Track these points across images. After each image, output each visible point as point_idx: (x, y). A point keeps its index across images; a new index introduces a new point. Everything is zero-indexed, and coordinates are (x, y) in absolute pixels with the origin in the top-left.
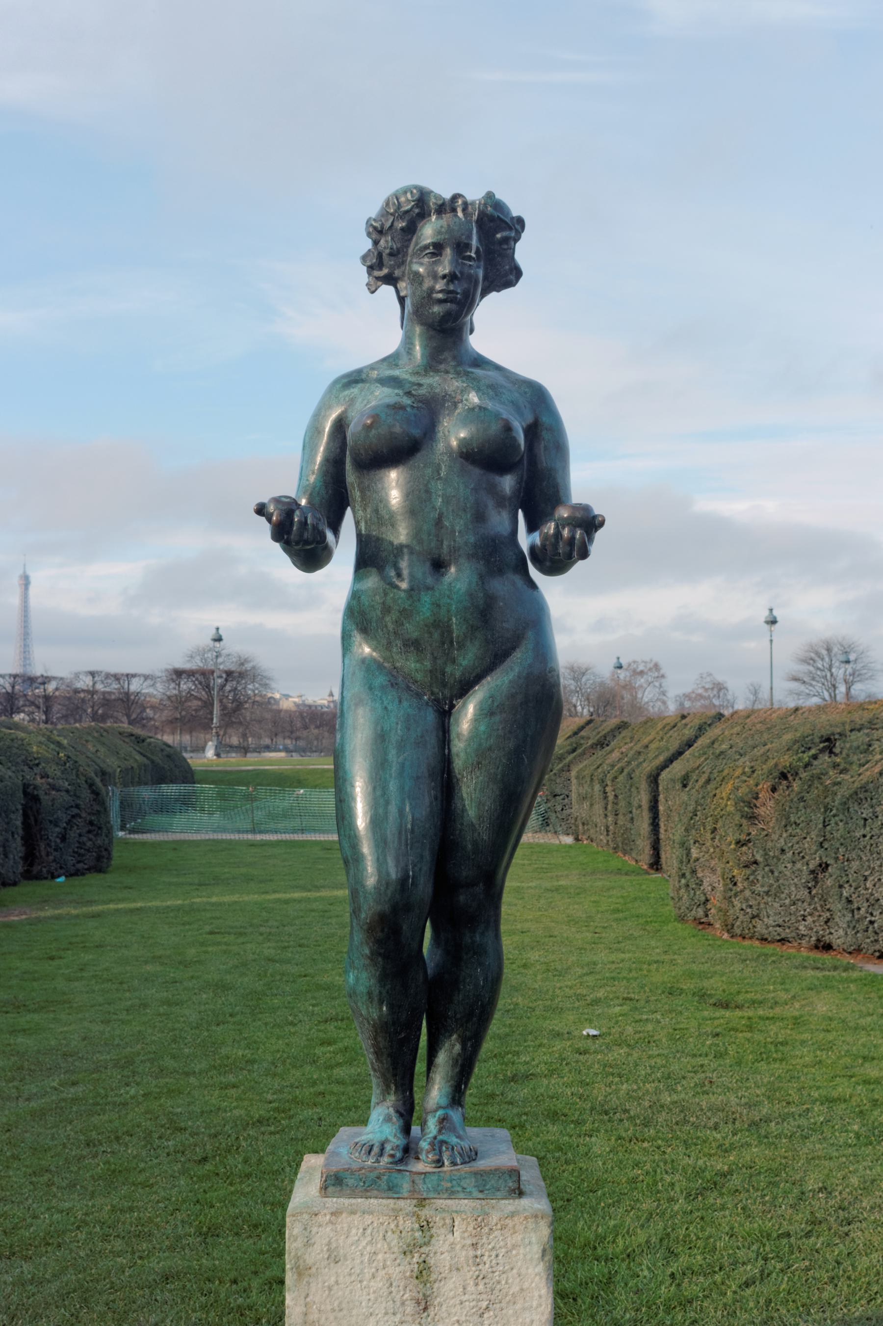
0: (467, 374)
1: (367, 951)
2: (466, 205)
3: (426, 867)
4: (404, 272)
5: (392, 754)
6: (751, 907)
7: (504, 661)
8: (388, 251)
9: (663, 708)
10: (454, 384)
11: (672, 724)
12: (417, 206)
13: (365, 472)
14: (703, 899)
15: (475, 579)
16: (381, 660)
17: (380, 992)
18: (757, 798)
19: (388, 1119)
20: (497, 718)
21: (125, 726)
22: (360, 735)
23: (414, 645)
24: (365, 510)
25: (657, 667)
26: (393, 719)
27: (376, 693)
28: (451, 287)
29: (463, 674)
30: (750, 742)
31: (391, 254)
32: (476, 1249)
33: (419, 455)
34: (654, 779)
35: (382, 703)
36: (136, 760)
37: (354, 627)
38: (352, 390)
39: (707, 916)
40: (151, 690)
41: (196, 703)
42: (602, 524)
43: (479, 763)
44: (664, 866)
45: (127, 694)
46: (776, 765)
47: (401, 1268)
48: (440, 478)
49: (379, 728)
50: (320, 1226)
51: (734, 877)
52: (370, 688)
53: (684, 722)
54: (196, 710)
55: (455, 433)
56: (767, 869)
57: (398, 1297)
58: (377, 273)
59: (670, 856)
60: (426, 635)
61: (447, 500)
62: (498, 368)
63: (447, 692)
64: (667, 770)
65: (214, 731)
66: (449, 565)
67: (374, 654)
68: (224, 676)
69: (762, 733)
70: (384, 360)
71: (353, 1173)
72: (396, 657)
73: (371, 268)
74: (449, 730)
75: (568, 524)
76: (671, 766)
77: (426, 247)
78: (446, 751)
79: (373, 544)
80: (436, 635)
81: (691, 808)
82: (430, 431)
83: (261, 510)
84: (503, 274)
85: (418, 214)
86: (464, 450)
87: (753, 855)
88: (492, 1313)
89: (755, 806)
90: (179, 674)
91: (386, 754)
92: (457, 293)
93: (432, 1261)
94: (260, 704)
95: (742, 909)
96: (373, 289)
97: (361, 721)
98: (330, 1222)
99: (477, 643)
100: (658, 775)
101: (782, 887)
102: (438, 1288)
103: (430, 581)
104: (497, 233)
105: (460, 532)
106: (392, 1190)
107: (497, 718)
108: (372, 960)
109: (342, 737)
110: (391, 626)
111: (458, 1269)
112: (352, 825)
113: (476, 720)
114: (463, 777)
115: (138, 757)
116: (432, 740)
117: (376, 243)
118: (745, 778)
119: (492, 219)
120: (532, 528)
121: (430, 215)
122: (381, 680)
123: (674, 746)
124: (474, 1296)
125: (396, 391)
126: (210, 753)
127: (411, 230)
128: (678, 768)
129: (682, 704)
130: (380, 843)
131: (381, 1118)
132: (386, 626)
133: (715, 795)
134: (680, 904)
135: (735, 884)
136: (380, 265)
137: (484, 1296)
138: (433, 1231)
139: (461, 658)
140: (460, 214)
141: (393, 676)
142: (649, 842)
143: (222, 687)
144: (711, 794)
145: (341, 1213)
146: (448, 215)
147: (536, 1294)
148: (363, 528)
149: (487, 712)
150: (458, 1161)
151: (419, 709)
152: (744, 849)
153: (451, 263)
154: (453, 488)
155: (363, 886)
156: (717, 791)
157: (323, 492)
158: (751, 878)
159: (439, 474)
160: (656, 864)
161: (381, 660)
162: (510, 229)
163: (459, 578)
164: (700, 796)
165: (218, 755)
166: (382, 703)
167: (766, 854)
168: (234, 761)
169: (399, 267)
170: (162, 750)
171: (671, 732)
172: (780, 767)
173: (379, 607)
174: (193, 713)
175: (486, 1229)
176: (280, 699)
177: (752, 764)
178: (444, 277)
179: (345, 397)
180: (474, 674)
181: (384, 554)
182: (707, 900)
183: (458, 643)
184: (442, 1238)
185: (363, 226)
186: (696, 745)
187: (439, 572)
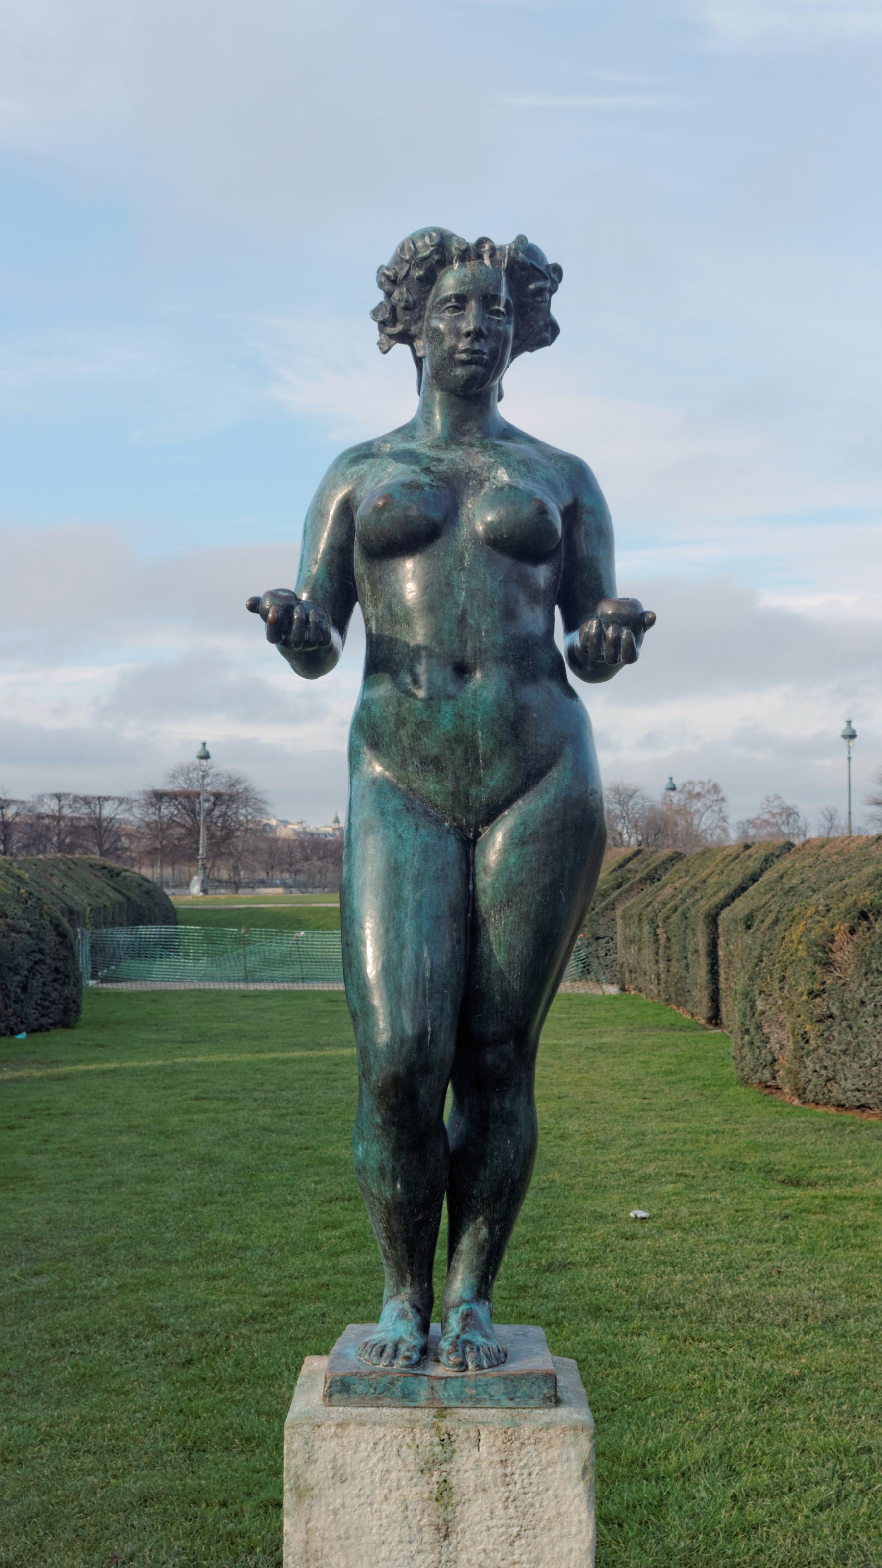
0: (495, 447)
1: (378, 1120)
2: (493, 251)
3: (447, 1022)
4: (421, 329)
5: (408, 890)
6: (825, 1068)
7: (538, 782)
8: (402, 304)
9: (723, 836)
10: (480, 459)
11: (734, 855)
12: (436, 251)
13: (376, 561)
14: (770, 1058)
15: (504, 686)
16: (395, 781)
17: (394, 1168)
18: (832, 941)
19: (403, 1315)
20: (530, 848)
21: (96, 857)
22: (370, 869)
23: (433, 763)
24: (376, 605)
25: (716, 788)
26: (409, 850)
27: (389, 818)
28: (477, 347)
29: (490, 797)
30: (825, 876)
31: (406, 308)
32: (505, 1467)
33: (438, 542)
34: (713, 919)
35: (396, 831)
36: (109, 897)
37: (363, 742)
38: (361, 466)
39: (774, 1078)
40: (126, 816)
41: (179, 831)
42: (652, 622)
43: (509, 900)
44: (724, 1020)
45: (99, 820)
46: (855, 903)
47: (419, 1488)
48: (463, 569)
49: (392, 860)
50: (324, 1439)
51: (805, 1033)
52: (382, 814)
53: (747, 852)
54: (179, 839)
55: (480, 516)
56: (844, 1024)
57: (415, 1522)
58: (390, 330)
59: (731, 1009)
60: (447, 752)
61: (471, 595)
62: (531, 440)
63: (472, 818)
64: (728, 908)
65: (200, 863)
66: (475, 670)
67: (387, 773)
68: (212, 799)
69: (838, 865)
70: (398, 431)
71: (361, 1377)
72: (413, 777)
73: (383, 324)
74: (474, 862)
75: (613, 623)
76: (732, 905)
77: (447, 300)
78: (471, 887)
79: (385, 645)
80: (459, 752)
81: (755, 953)
82: (452, 514)
83: (255, 606)
84: (538, 331)
85: (438, 262)
86: (492, 536)
87: (828, 1008)
88: (523, 1541)
89: (831, 950)
90: (159, 796)
91: (400, 889)
92: (484, 354)
93: (453, 1481)
94: (253, 832)
95: (815, 1071)
96: (386, 348)
97: (372, 851)
98: (336, 1435)
99: (506, 761)
100: (718, 914)
101: (862, 1045)
102: (462, 1512)
103: (451, 688)
104: (530, 283)
105: (486, 632)
106: (407, 1398)
107: (530, 848)
108: (384, 1130)
109: (350, 871)
110: (406, 741)
111: (484, 1490)
112: (360, 973)
113: (506, 850)
114: (490, 916)
115: (112, 894)
116: (454, 874)
117: (389, 295)
118: (819, 918)
119: (523, 266)
120: (570, 626)
121: (451, 263)
122: (394, 804)
123: (736, 881)
124: (503, 1522)
125: (413, 467)
126: (195, 889)
127: (430, 279)
128: (740, 907)
129: (745, 832)
130: (394, 994)
131: (395, 1314)
132: (401, 741)
133: (784, 938)
134: (743, 1064)
135: (807, 1042)
136: (393, 320)
137: (515, 1522)
138: (455, 1445)
139: (488, 778)
140: (487, 261)
141: (408, 799)
142: (706, 992)
143: (210, 812)
144: (779, 937)
145: (348, 1424)
146: (473, 262)
147: (575, 1519)
148: (374, 627)
149: (517, 841)
150: (485, 1364)
151: (439, 838)
152: (818, 1000)
153: (476, 318)
154: (479, 581)
155: (374, 1044)
156: (787, 934)
157: (327, 585)
158: (826, 1034)
159: (462, 564)
160: (715, 1019)
161: (395, 781)
162: (545, 278)
163: (485, 685)
164: (767, 939)
165: (205, 891)
166: (396, 831)
167: (843, 1007)
168: (223, 898)
169: (415, 323)
170: (140, 886)
171: (733, 864)
172: (860, 905)
173: (392, 719)
174: (176, 842)
175: (517, 1444)
176: (277, 826)
177: (827, 902)
178: (468, 334)
179: (352, 474)
180: (503, 797)
181: (398, 658)
182: (775, 1060)
183: (484, 760)
184: (465, 1454)
185: (374, 275)
186: (761, 879)
187: (462, 678)
